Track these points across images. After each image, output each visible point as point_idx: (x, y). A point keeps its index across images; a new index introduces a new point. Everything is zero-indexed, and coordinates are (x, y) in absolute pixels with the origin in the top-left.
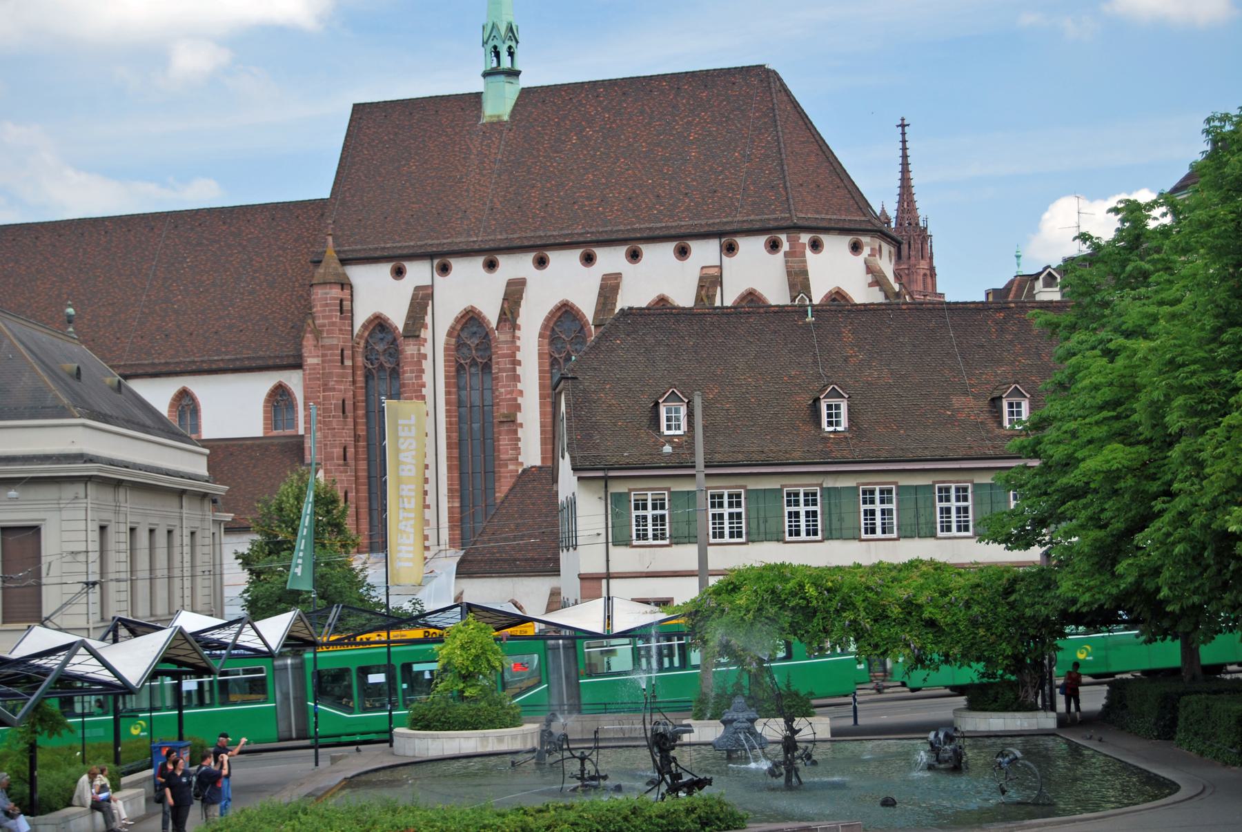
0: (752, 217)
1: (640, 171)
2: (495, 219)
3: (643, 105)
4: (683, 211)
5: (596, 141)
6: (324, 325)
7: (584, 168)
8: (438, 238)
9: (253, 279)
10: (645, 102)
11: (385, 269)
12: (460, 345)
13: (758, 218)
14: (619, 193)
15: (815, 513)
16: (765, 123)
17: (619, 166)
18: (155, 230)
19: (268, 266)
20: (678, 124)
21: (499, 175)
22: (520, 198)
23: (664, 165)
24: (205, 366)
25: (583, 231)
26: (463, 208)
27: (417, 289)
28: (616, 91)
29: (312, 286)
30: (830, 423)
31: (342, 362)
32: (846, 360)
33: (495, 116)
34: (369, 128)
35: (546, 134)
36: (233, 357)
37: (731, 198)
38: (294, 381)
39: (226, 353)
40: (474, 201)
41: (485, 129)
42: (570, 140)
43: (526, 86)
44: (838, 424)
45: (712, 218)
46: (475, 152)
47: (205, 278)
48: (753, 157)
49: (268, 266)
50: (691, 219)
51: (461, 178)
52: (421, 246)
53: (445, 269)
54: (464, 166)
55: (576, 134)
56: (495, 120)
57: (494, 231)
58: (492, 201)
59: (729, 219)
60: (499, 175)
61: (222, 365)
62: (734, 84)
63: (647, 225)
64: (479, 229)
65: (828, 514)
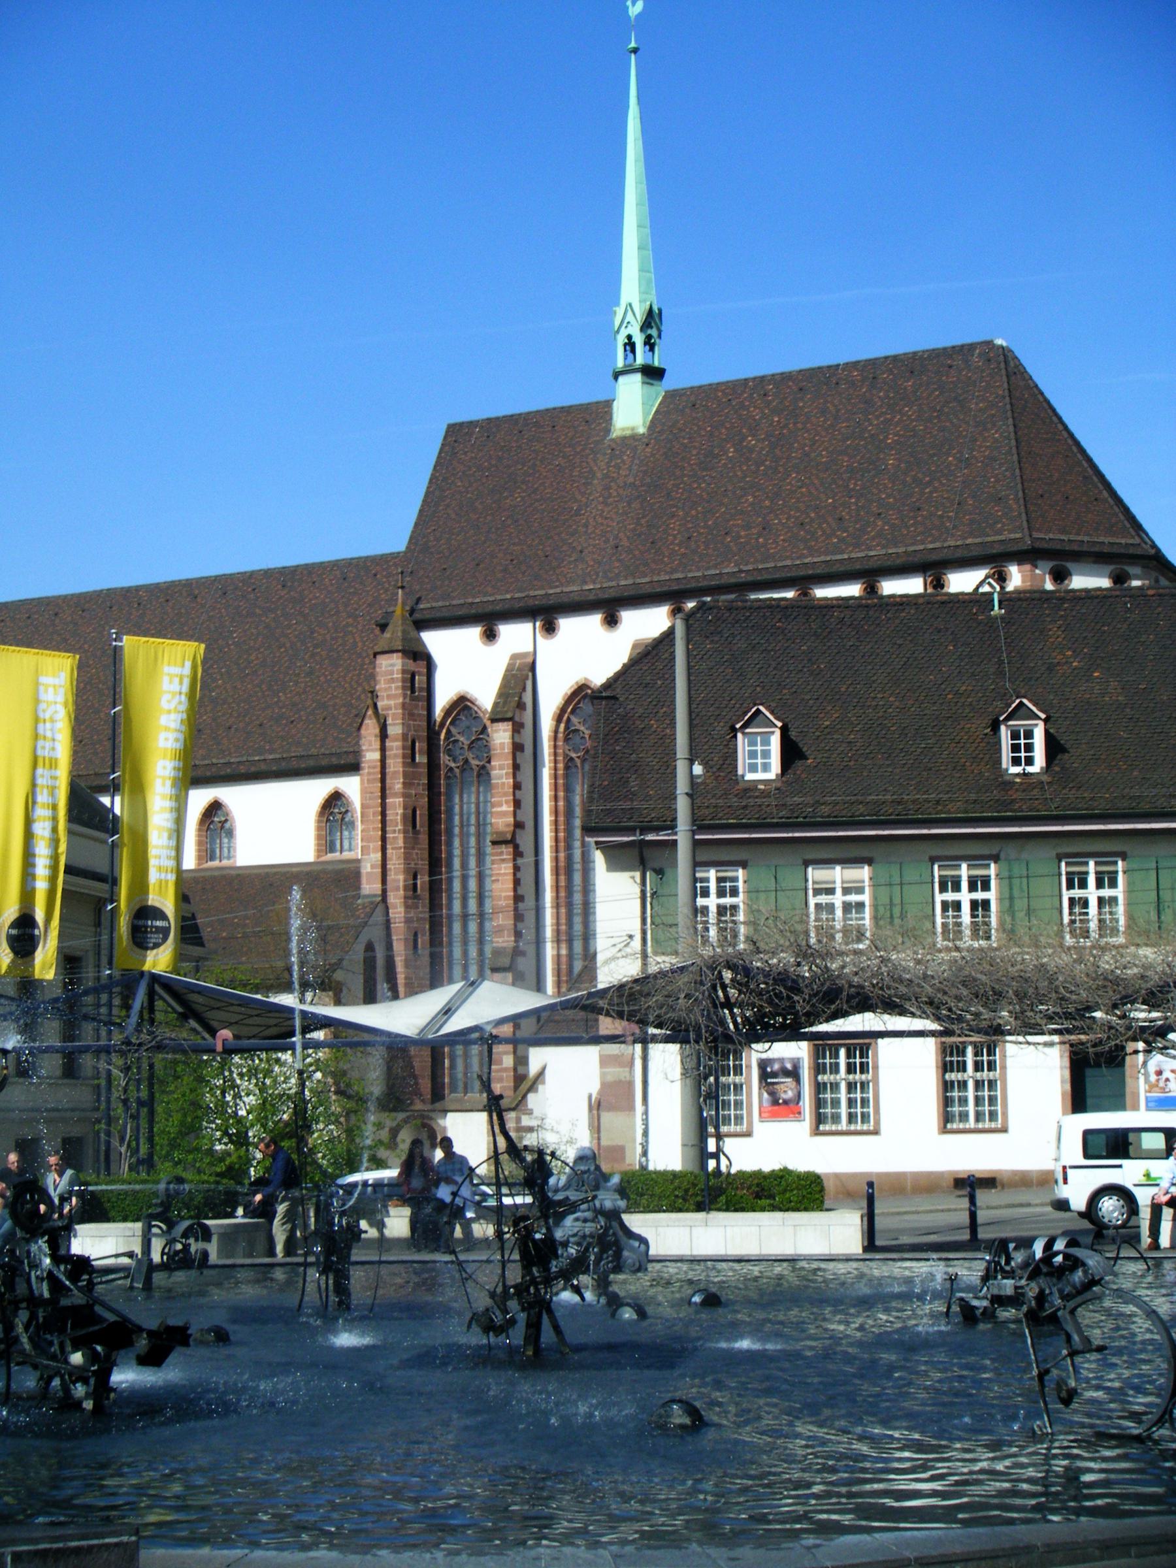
0: (969, 541)
1: (817, 489)
2: (620, 561)
3: (826, 402)
4: (873, 538)
5: (760, 452)
6: (389, 708)
7: (742, 489)
8: (542, 588)
9: (313, 655)
10: (829, 399)
11: (473, 633)
12: (570, 733)
13: (978, 540)
14: (788, 519)
15: (986, 904)
16: (993, 416)
17: (790, 483)
18: (199, 600)
19: (333, 639)
20: (870, 424)
21: (629, 504)
22: (654, 531)
23: (850, 478)
24: (243, 769)
25: (736, 570)
26: (579, 548)
27: (514, 657)
28: (789, 387)
29: (375, 655)
30: (1016, 761)
31: (413, 758)
32: (1051, 669)
33: (628, 429)
34: (465, 453)
35: (695, 447)
36: (278, 756)
37: (941, 517)
38: (351, 786)
39: (271, 751)
40: (594, 539)
41: (614, 446)
42: (726, 453)
43: (671, 388)
44: (1030, 761)
45: (913, 544)
46: (599, 475)
47: (253, 657)
48: (973, 461)
49: (333, 639)
50: (883, 547)
51: (579, 510)
52: (520, 599)
53: (550, 629)
54: (583, 494)
55: (733, 446)
56: (628, 433)
57: (617, 576)
58: (616, 537)
59: (938, 545)
60: (629, 504)
61: (263, 767)
62: (950, 367)
63: (822, 558)
64: (597, 574)
65: (1009, 901)
